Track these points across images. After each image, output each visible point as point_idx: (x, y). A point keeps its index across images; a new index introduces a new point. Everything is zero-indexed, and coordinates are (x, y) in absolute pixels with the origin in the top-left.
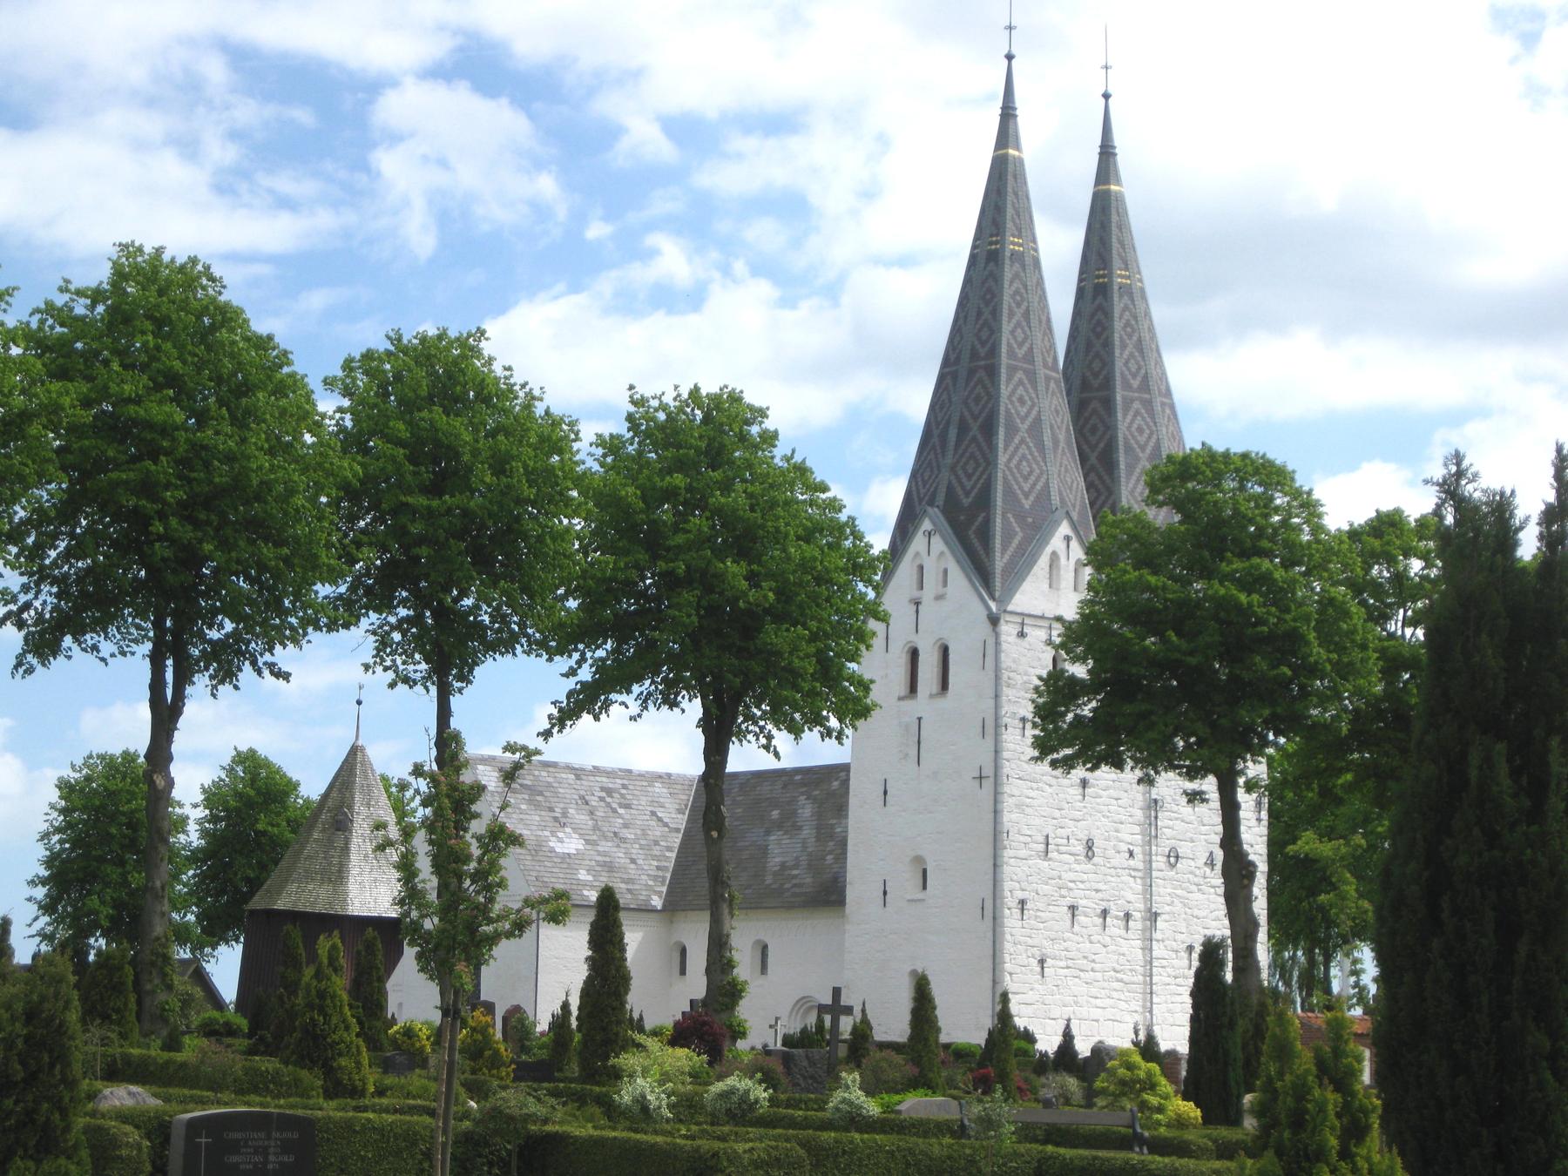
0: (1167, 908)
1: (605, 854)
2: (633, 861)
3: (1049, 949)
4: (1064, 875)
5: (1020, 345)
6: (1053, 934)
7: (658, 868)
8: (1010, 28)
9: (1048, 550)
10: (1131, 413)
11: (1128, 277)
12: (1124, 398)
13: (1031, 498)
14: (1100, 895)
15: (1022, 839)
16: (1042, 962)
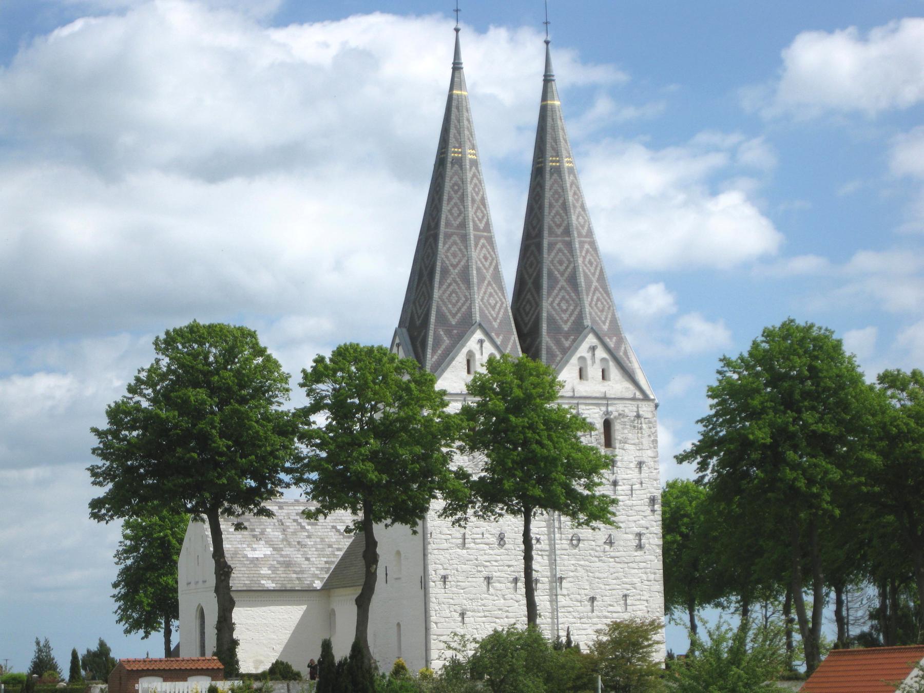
0: (572, 574)
1: (287, 556)
2: (307, 559)
3: (468, 605)
4: (480, 558)
5: (480, 221)
6: (472, 596)
7: (326, 562)
8: (457, 11)
9: (465, 351)
10: (555, 251)
11: (558, 161)
12: (475, 236)
13: (569, 324)
14: (512, 569)
15: (443, 537)
16: (462, 615)
